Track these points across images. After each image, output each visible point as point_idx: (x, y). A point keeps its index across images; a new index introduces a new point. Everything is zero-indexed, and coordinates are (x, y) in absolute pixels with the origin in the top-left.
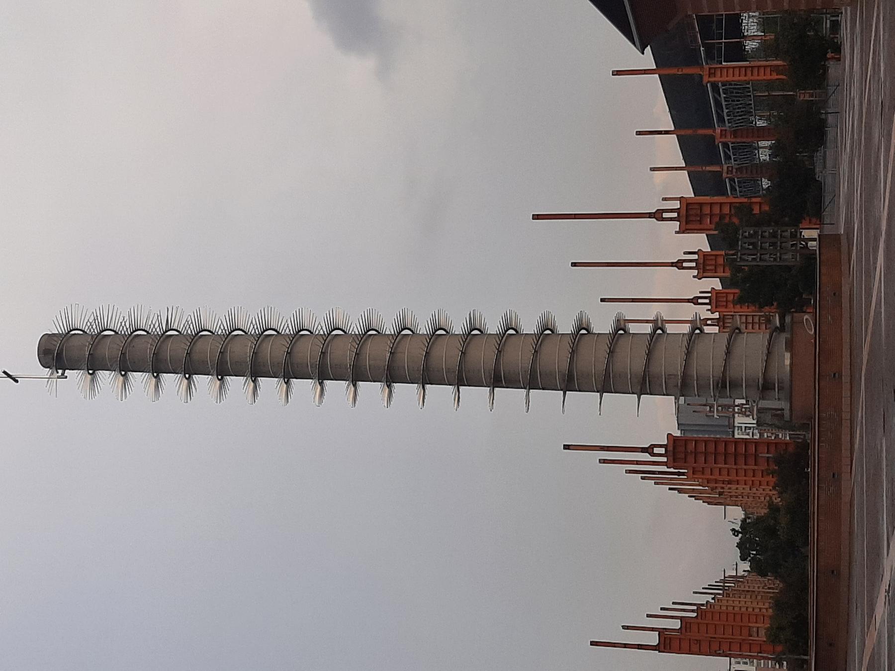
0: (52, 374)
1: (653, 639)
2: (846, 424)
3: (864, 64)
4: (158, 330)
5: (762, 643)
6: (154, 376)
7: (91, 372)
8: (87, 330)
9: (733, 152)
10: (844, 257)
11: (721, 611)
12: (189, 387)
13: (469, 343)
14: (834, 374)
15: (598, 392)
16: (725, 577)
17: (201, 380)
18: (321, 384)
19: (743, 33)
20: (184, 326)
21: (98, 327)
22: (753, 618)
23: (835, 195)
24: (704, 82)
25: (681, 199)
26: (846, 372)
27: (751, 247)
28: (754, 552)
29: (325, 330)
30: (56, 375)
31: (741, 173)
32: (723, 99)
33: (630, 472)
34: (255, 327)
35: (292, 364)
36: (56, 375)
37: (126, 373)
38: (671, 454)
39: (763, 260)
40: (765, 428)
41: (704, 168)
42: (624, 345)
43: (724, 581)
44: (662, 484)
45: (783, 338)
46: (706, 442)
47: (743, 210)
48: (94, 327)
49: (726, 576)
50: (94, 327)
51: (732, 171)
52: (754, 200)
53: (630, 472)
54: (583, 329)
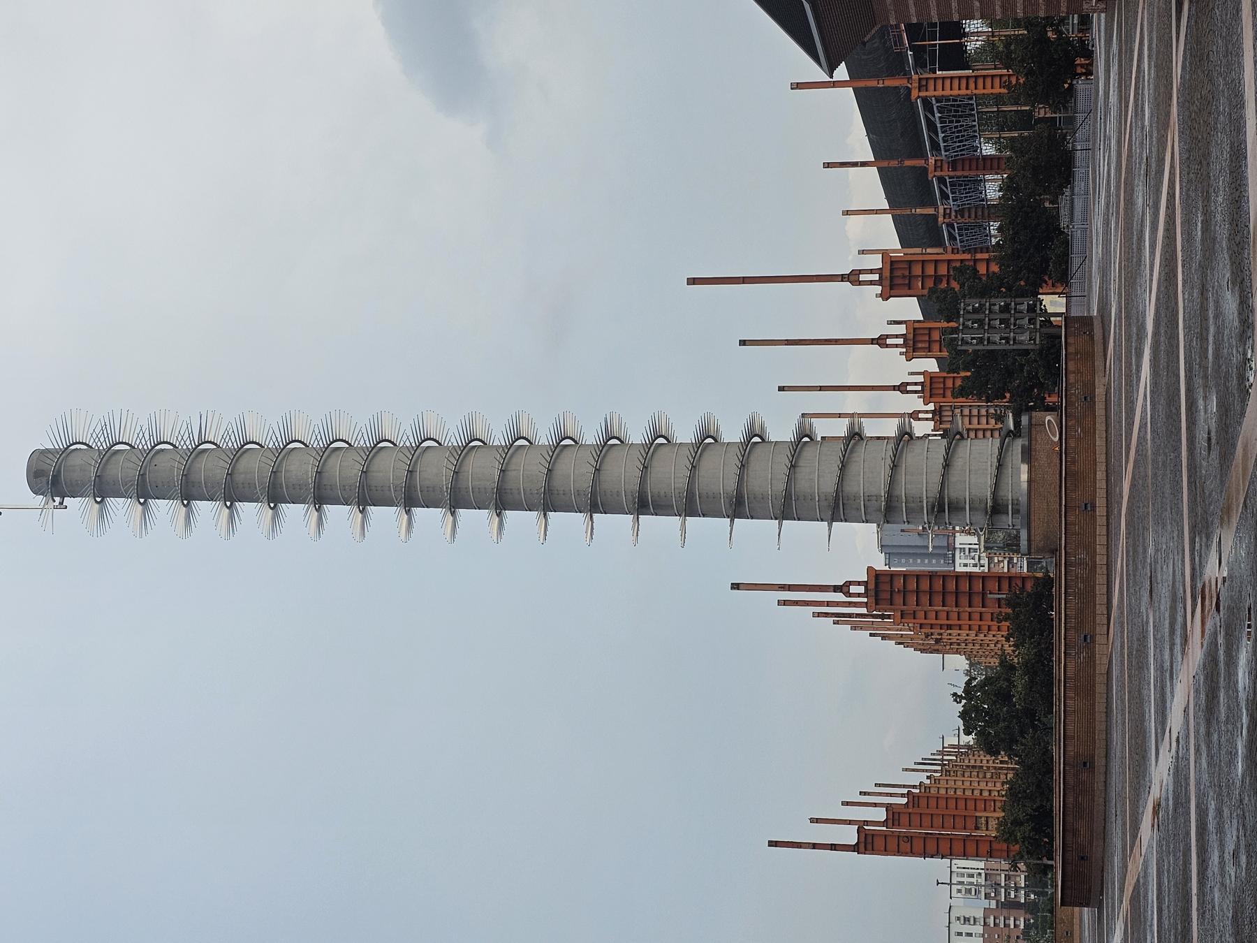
1: (850, 835)
2: (1101, 571)
3: (1123, 99)
4: (188, 442)
5: (992, 839)
6: (183, 503)
8: (93, 444)
9: (951, 189)
10: (1098, 348)
11: (939, 796)
12: (231, 518)
13: (604, 456)
14: (1086, 505)
15: (776, 519)
16: (943, 748)
17: (247, 509)
18: (408, 512)
19: (964, 29)
20: (223, 437)
21: (107, 439)
22: (981, 805)
23: (1086, 257)
24: (913, 98)
25: (885, 253)
26: (1100, 502)
29: (412, 440)
30: (51, 504)
31: (962, 217)
32: (937, 120)
34: (319, 438)
35: (369, 487)
36: (51, 504)
37: (145, 501)
39: (992, 327)
40: (995, 551)
41: (913, 210)
42: (810, 456)
43: (942, 753)
45: (1018, 444)
46: (918, 576)
47: (965, 272)
48: (102, 439)
49: (945, 746)
50: (102, 439)
51: (950, 214)
52: (979, 256)
53: (819, 615)
54: (755, 437)
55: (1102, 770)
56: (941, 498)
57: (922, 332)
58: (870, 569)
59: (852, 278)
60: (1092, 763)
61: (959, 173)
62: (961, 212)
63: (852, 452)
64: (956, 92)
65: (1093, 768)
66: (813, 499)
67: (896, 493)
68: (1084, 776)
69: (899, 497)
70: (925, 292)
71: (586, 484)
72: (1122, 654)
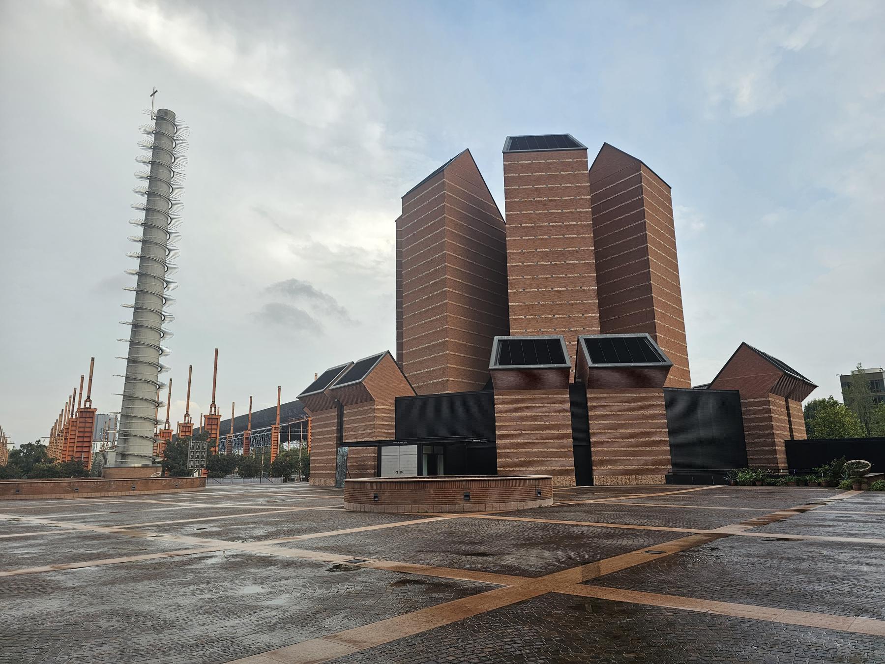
0: (154, 114)
2: (106, 494)
7: (154, 132)
10: (194, 489)
18: (140, 241)
26: (135, 493)
27: (198, 447)
28: (25, 452)
30: (154, 115)
33: (75, 390)
35: (152, 228)
36: (154, 115)
38: (86, 410)
43: (4, 437)
44: (66, 406)
45: (150, 463)
47: (213, 444)
53: (75, 390)
54: (160, 368)
55: (15, 498)
56: (130, 435)
57: (216, 422)
58: (96, 409)
59: (213, 405)
60: (18, 494)
61: (244, 441)
62: (230, 442)
63: (152, 403)
64: (273, 439)
65: (17, 494)
66: (134, 389)
67: (134, 419)
68: (12, 491)
69: (132, 420)
70: (206, 430)
71: (147, 306)
72: (71, 504)
